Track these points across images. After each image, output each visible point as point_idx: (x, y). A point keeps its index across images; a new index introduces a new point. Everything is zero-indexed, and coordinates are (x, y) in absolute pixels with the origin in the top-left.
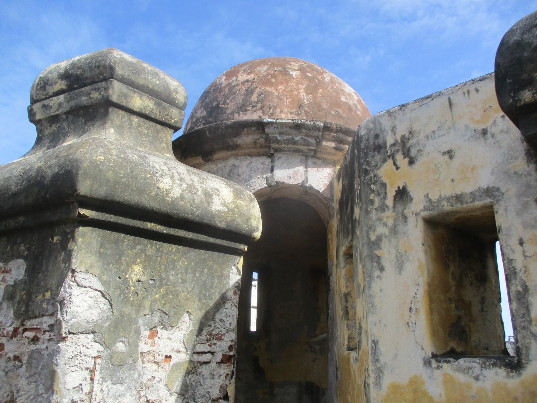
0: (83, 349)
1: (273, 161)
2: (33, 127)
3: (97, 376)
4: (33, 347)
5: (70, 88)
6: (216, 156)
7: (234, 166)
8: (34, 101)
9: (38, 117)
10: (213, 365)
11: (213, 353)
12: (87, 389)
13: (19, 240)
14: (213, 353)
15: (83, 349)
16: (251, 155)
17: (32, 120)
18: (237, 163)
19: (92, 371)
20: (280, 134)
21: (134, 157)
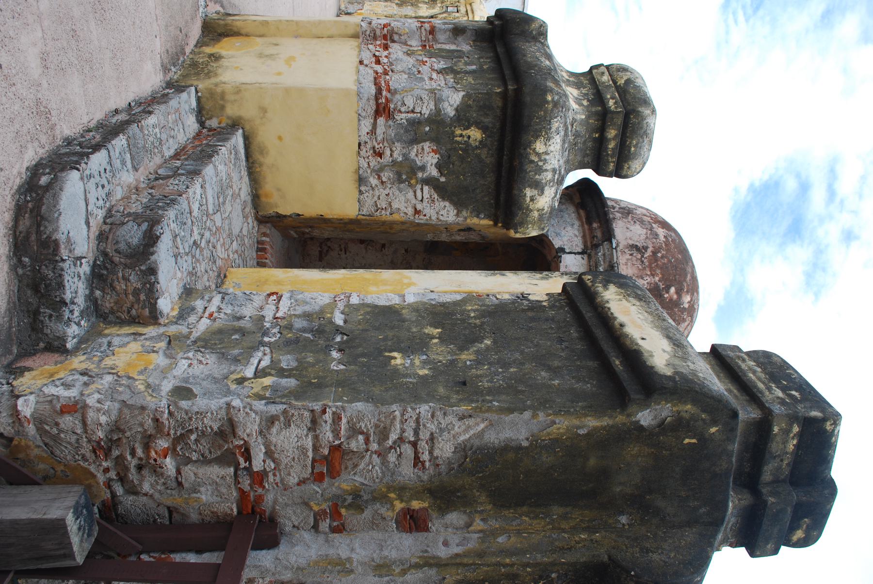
0: (426, 104)
1: (579, 253)
2: (587, 69)
3: (410, 115)
4: (426, 79)
5: (618, 88)
6: (582, 212)
7: (573, 225)
8: (608, 67)
9: (594, 71)
10: (414, 201)
11: (422, 201)
12: (403, 109)
13: (522, 151)
14: (422, 201)
15: (426, 104)
16: (584, 237)
17: (592, 68)
18: (576, 227)
19: (413, 112)
20: (604, 255)
21: (556, 124)
